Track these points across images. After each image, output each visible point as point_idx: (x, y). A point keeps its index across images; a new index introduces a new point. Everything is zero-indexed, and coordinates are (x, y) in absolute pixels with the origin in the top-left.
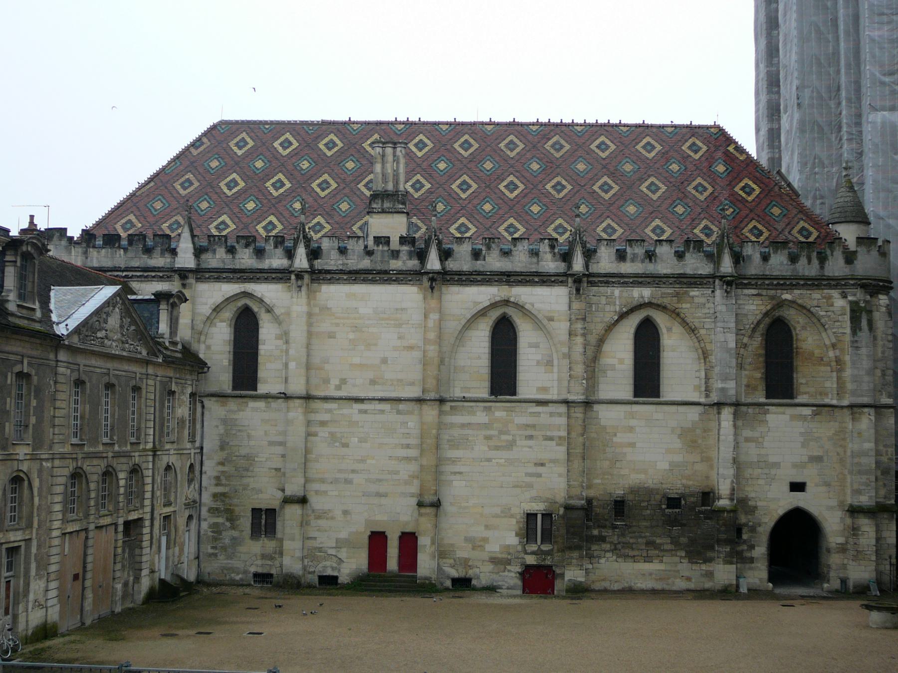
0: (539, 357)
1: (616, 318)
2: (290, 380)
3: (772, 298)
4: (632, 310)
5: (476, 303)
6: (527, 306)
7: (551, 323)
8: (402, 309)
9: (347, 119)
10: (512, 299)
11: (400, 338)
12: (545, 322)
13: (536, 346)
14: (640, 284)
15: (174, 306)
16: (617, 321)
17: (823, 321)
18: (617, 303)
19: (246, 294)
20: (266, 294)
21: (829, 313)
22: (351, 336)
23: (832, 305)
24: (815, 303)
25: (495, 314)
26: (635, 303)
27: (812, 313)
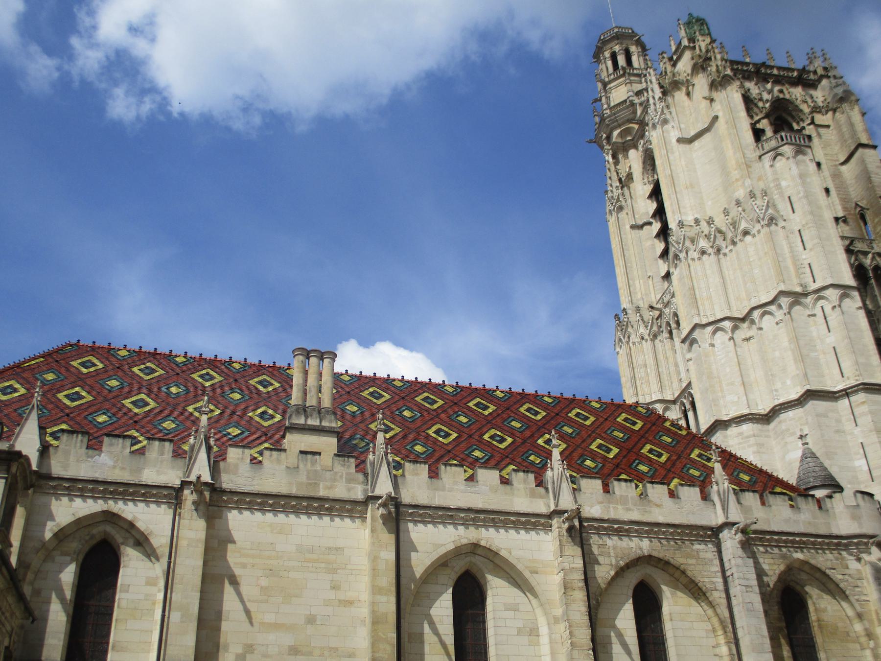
0: (520, 624)
1: (612, 573)
2: (812, 318)
3: (784, 557)
4: (628, 566)
5: (437, 546)
6: (503, 553)
7: (535, 575)
8: (337, 549)
9: (213, 357)
10: (483, 543)
11: (333, 588)
12: (527, 574)
13: (515, 608)
14: (639, 535)
15: (322, 359)
16: (613, 579)
17: (842, 585)
18: (612, 554)
19: (110, 517)
20: (139, 516)
21: (847, 577)
22: (264, 582)
23: (847, 568)
24: (829, 564)
25: (459, 567)
26: (633, 556)
27: (828, 576)
